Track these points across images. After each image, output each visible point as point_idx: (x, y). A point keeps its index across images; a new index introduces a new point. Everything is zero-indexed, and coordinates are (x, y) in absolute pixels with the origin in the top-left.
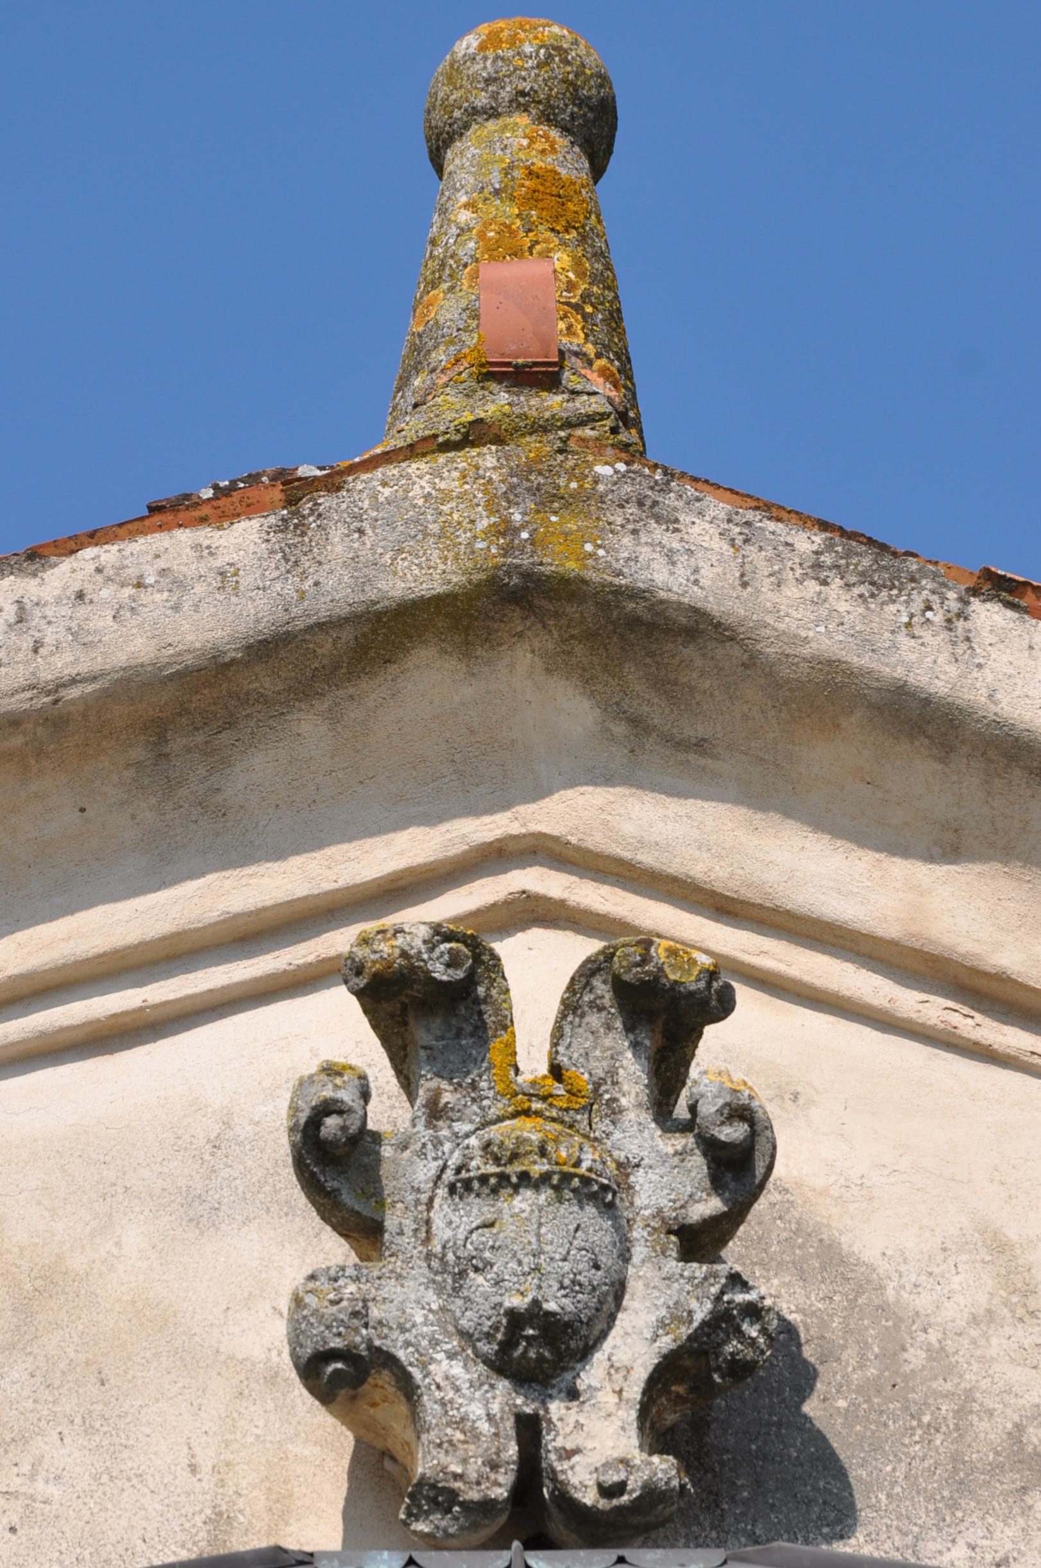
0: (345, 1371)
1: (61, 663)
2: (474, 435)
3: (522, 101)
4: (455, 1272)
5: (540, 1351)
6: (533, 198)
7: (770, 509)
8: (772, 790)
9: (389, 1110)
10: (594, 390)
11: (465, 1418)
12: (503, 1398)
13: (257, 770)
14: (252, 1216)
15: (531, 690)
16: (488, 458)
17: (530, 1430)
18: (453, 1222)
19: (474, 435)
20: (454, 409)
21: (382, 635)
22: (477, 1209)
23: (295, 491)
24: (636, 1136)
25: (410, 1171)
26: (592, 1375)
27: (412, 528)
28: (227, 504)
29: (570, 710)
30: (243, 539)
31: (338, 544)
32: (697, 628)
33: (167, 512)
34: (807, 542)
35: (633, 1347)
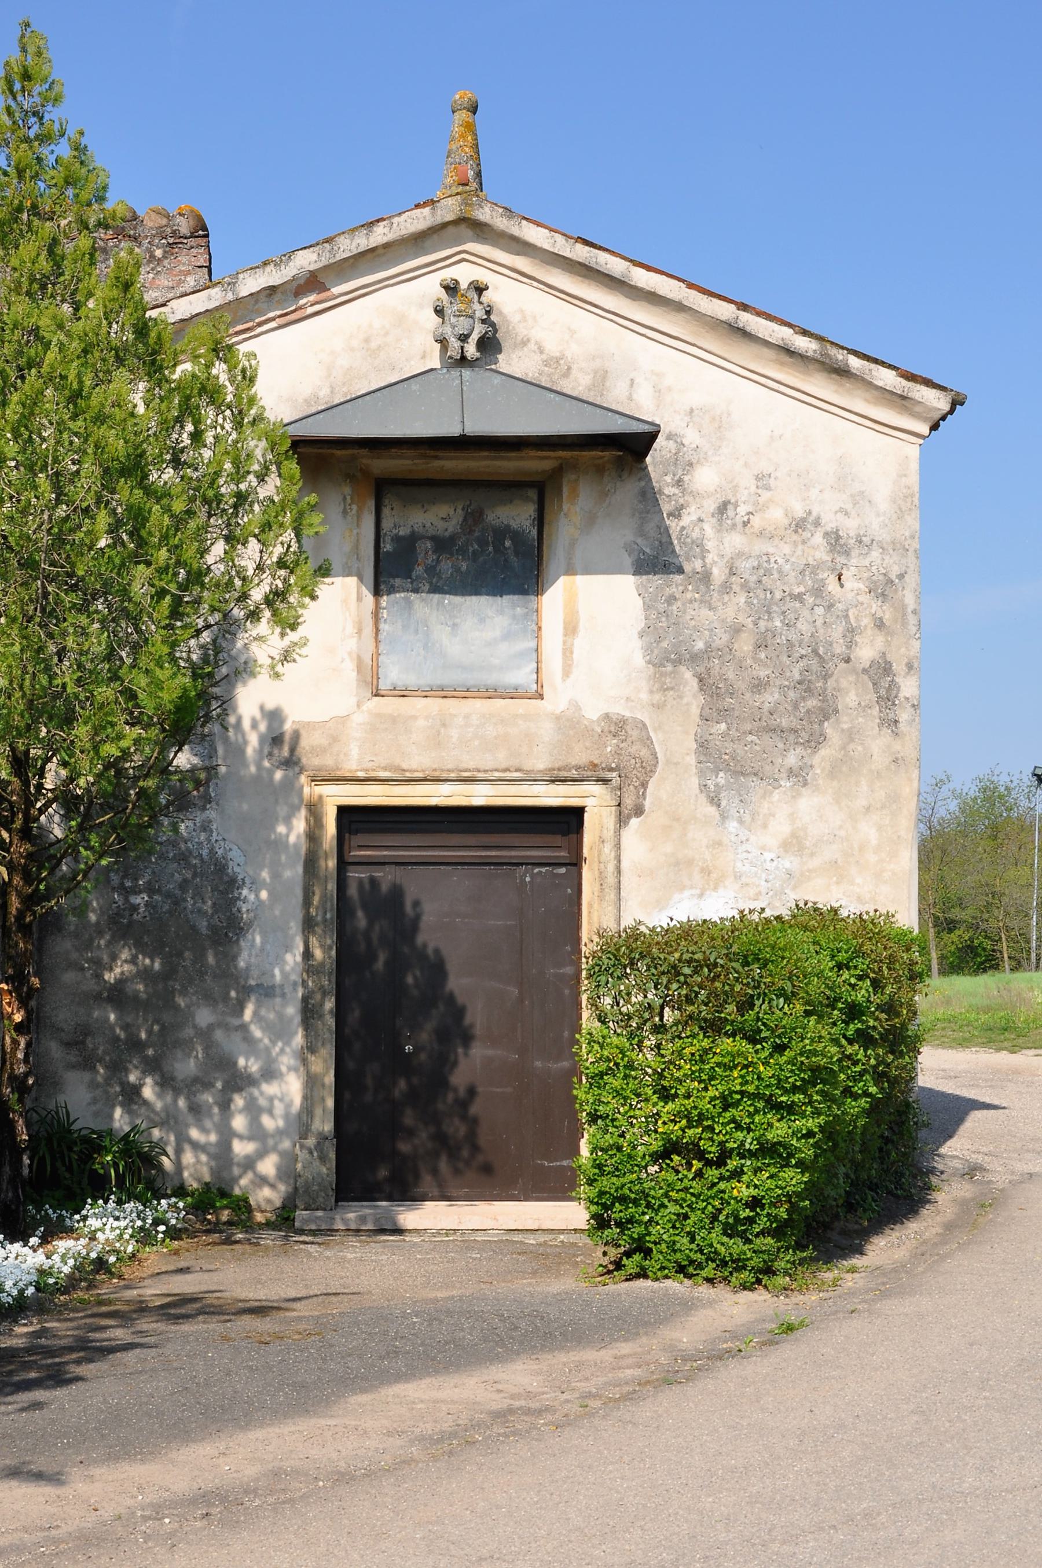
0: (443, 342)
1: (403, 232)
2: (458, 194)
3: (464, 108)
4: (453, 327)
5: (464, 338)
6: (466, 127)
7: (496, 204)
8: (495, 244)
9: (446, 303)
10: (474, 185)
11: (455, 344)
12: (459, 343)
13: (428, 243)
14: (496, 1556)
15: (464, 230)
16: (459, 197)
17: (462, 348)
18: (453, 320)
19: (458, 194)
20: (454, 190)
21: (444, 226)
22: (456, 319)
23: (433, 202)
24: (476, 306)
25: (448, 311)
26: (470, 340)
27: (449, 209)
28: (425, 204)
29: (469, 233)
30: (426, 211)
31: (439, 212)
32: (486, 225)
33: (418, 206)
34: (501, 210)
35: (475, 337)
